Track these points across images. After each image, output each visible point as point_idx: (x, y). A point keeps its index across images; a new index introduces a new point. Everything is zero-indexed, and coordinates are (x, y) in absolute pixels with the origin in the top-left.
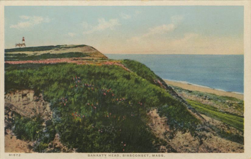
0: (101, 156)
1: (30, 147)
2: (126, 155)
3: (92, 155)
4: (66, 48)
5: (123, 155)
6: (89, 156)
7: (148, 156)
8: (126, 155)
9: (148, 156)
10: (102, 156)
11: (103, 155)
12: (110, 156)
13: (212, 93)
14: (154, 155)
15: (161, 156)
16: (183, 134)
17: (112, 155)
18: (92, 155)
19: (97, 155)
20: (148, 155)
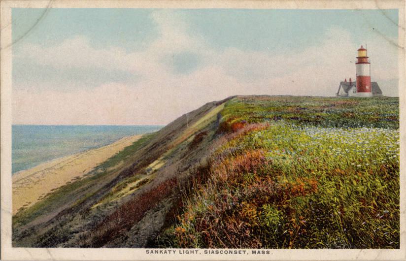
0: (166, 253)
1: (99, 176)
2: (209, 251)
3: (152, 251)
4: (35, 25)
5: (146, 251)
6: (148, 252)
7: (244, 253)
8: (209, 251)
9: (244, 253)
10: (168, 252)
11: (170, 251)
12: (193, 252)
13: (152, 144)
14: (255, 251)
15: (266, 252)
16: (365, 55)
17: (239, 251)
18: (152, 251)
19: (161, 252)
20: (244, 251)
